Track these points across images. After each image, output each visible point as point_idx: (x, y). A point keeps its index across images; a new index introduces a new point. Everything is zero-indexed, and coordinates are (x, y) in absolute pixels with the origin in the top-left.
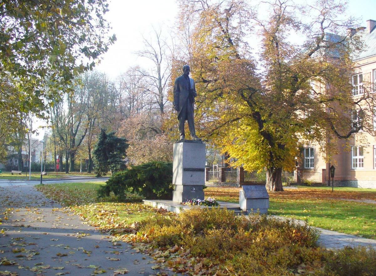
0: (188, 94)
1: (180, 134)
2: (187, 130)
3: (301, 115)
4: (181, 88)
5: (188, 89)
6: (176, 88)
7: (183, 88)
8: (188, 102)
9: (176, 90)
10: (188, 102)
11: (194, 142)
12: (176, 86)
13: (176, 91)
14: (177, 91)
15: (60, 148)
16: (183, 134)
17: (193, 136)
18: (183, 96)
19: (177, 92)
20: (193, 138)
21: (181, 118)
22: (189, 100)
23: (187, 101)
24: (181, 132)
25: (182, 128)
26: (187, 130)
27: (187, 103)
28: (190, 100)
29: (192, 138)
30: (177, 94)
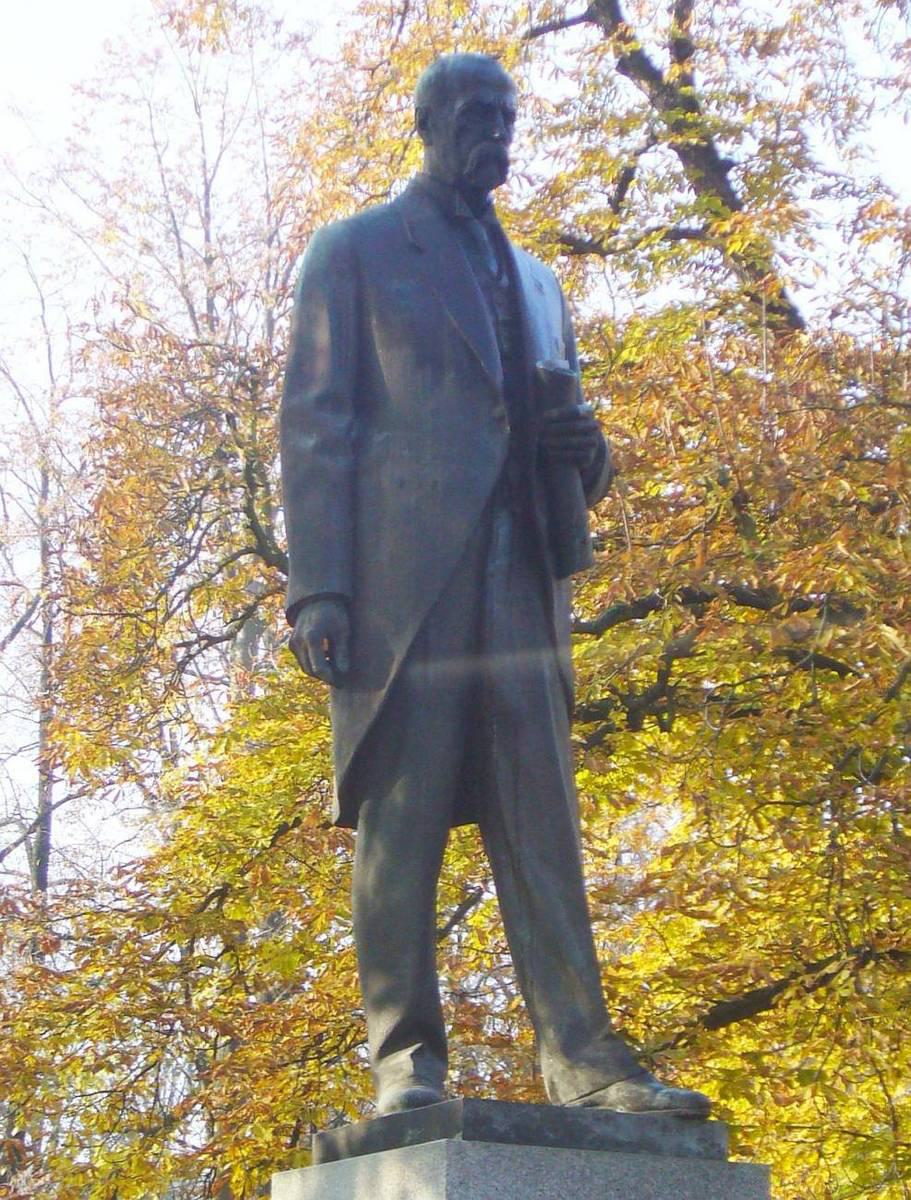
0: (497, 443)
1: (380, 1027)
2: (476, 953)
3: (665, 716)
4: (391, 364)
5: (499, 378)
6: (322, 365)
7: (426, 360)
8: (499, 563)
9: (315, 391)
10: (499, 563)
11: (603, 1144)
12: (323, 336)
13: (322, 401)
14: (327, 401)
15: (603, 681)
16: (422, 1030)
17: (571, 1049)
18: (429, 476)
19: (340, 422)
20: (583, 1078)
21: (398, 795)
22: (503, 531)
23: (484, 548)
24: (379, 1004)
25: (401, 946)
26: (476, 953)
27: (481, 580)
28: (525, 525)
29: (562, 1082)
30: (325, 447)
